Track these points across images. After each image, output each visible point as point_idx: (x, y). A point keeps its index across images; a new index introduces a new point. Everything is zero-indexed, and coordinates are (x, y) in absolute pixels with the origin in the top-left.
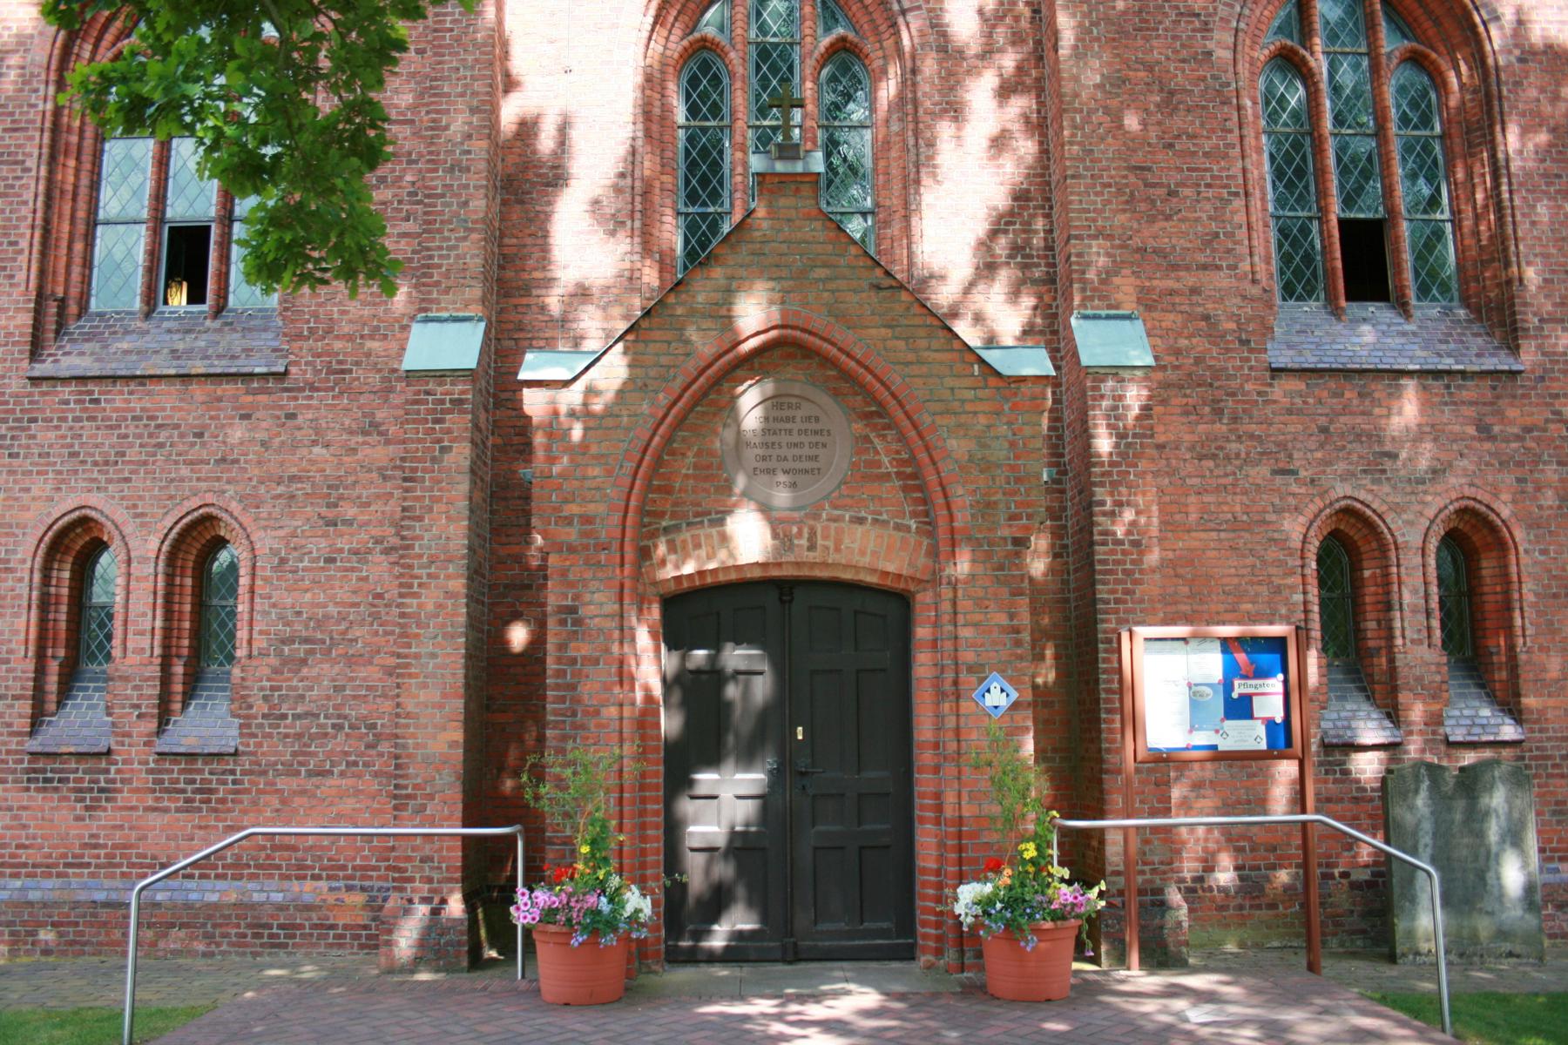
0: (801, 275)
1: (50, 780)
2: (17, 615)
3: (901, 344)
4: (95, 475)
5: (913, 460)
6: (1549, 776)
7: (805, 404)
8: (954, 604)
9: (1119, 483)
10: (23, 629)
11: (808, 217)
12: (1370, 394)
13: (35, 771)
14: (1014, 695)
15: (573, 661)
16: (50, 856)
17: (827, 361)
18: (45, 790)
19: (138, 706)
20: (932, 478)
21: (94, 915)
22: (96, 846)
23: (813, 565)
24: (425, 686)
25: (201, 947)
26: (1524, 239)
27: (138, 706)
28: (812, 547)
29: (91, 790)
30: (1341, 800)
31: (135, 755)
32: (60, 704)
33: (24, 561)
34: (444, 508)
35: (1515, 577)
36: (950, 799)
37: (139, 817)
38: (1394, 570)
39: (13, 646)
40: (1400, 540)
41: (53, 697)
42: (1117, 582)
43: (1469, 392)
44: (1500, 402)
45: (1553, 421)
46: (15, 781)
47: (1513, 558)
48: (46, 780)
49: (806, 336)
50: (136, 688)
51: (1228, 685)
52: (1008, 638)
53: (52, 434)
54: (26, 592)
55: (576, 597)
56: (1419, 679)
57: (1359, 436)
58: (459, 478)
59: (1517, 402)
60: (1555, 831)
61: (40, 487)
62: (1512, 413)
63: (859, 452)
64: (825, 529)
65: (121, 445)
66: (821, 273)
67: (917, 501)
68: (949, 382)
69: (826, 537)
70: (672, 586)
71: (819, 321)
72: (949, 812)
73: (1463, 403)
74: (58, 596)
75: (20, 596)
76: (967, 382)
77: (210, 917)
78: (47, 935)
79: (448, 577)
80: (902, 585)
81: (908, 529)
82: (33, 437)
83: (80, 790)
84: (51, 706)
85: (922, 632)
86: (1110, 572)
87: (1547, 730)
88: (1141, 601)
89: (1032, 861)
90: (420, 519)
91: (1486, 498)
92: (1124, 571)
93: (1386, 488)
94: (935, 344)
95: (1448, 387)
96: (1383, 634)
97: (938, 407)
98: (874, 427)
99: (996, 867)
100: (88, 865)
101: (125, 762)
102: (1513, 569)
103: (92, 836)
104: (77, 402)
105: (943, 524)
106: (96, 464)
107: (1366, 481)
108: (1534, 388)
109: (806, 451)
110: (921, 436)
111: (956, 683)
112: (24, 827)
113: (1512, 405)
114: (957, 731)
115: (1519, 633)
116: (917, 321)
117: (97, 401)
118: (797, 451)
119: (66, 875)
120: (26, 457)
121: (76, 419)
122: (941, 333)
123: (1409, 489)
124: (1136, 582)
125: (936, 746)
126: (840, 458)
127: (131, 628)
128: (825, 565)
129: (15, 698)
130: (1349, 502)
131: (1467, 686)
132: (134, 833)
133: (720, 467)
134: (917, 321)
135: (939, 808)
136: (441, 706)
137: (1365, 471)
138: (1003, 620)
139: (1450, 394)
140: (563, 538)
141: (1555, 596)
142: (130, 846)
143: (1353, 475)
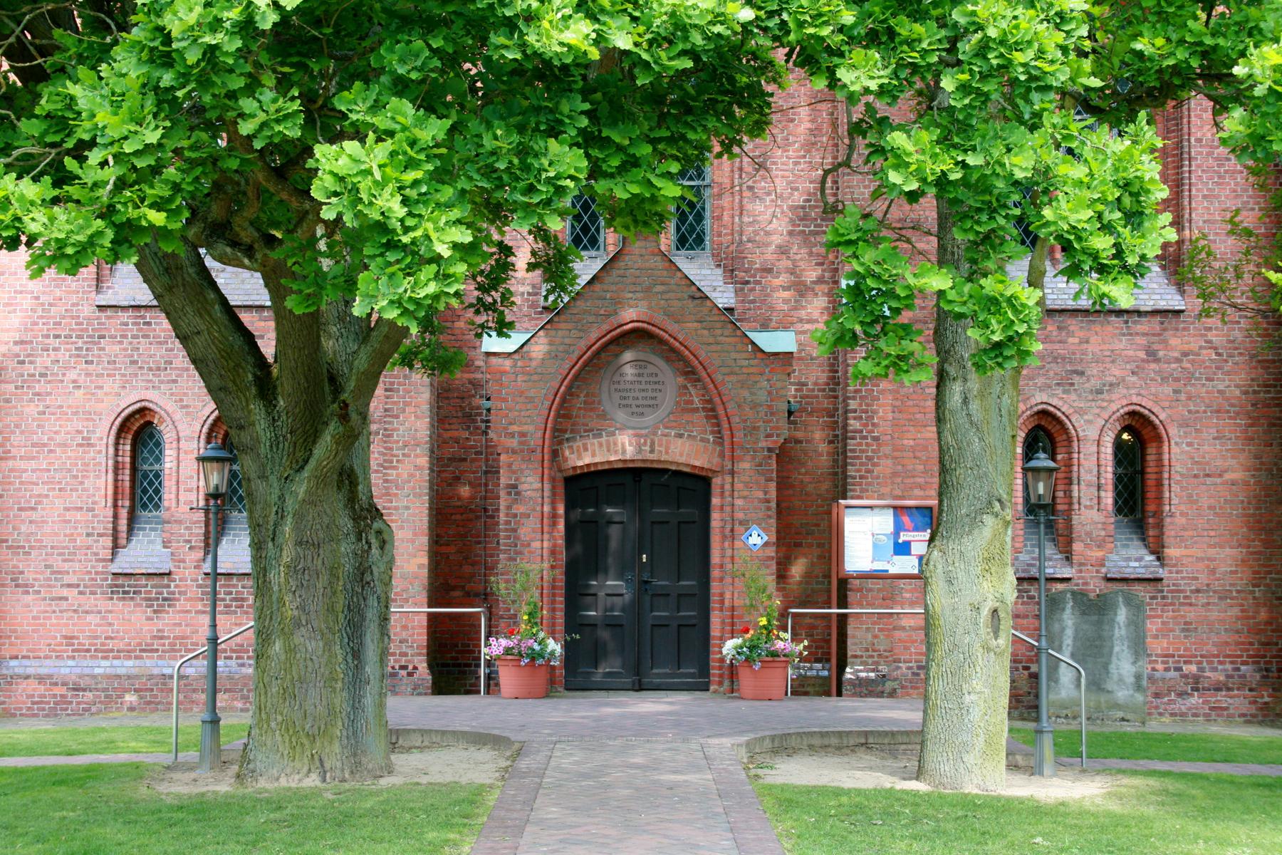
0: (648, 290)
1: (128, 593)
2: (98, 477)
3: (706, 332)
4: (151, 377)
5: (710, 401)
6: (1181, 604)
7: (649, 366)
8: (733, 485)
9: (866, 397)
10: (103, 487)
11: (653, 254)
12: (1066, 328)
13: (116, 586)
14: (766, 538)
15: (515, 516)
16: (129, 644)
17: (661, 341)
18: (124, 599)
19: (189, 541)
20: (722, 412)
21: (164, 684)
22: (162, 638)
23: (652, 461)
24: (402, 528)
25: (240, 705)
26: (1196, 209)
27: (189, 541)
28: (652, 451)
29: (158, 599)
30: (1027, 616)
31: (190, 575)
32: (128, 540)
33: (101, 439)
34: (413, 409)
35: (1166, 462)
36: (728, 596)
37: (192, 618)
38: (1076, 456)
39: (97, 499)
40: (1081, 434)
41: (124, 535)
42: (862, 464)
43: (1144, 325)
44: (1166, 333)
45: (1205, 348)
46: (102, 593)
47: (1166, 448)
48: (124, 592)
49: (650, 327)
50: (187, 528)
51: (896, 534)
52: (763, 506)
53: (117, 347)
54: (104, 461)
55: (517, 479)
56: (1089, 534)
57: (1056, 358)
58: (423, 389)
59: (1179, 334)
60: (1183, 643)
61: (110, 385)
62: (1174, 342)
63: (681, 395)
64: (660, 441)
65: (169, 356)
66: (659, 288)
67: (713, 425)
68: (734, 355)
69: (660, 445)
70: (571, 473)
71: (659, 318)
72: (727, 604)
73: (1137, 334)
74: (123, 463)
75: (100, 464)
76: (745, 355)
77: (245, 685)
78: (130, 698)
79: (416, 456)
80: (704, 474)
81: (708, 441)
82: (103, 349)
83: (150, 599)
84: (123, 541)
85: (715, 501)
86: (857, 457)
87: (1181, 572)
88: (878, 477)
89: (764, 627)
90: (397, 417)
91: (1149, 405)
92: (867, 457)
93: (1074, 396)
94: (726, 333)
95: (1127, 322)
96: (1066, 500)
97: (727, 370)
98: (690, 381)
99: (747, 631)
100: (157, 651)
101: (181, 580)
102: (1166, 457)
103: (159, 631)
104: (135, 324)
105: (727, 440)
106: (150, 369)
107: (1059, 391)
108: (1193, 323)
109: (650, 394)
110: (716, 387)
111: (732, 530)
112: (110, 624)
113: (1175, 336)
114: (732, 558)
115: (1167, 502)
116: (716, 318)
117: (149, 324)
118: (644, 394)
119: (141, 658)
120: (98, 364)
121: (134, 337)
122: (730, 326)
123: (1090, 397)
124: (875, 465)
125: (721, 566)
126: (669, 397)
127: (182, 487)
128: (659, 461)
129: (100, 535)
130: (1044, 406)
131: (1132, 539)
132: (189, 629)
133: (599, 403)
134: (716, 318)
135: (722, 602)
136: (413, 541)
137: (1058, 384)
138: (761, 495)
139: (1128, 328)
140: (509, 445)
141: (1196, 476)
142: (187, 638)
143: (1050, 387)
